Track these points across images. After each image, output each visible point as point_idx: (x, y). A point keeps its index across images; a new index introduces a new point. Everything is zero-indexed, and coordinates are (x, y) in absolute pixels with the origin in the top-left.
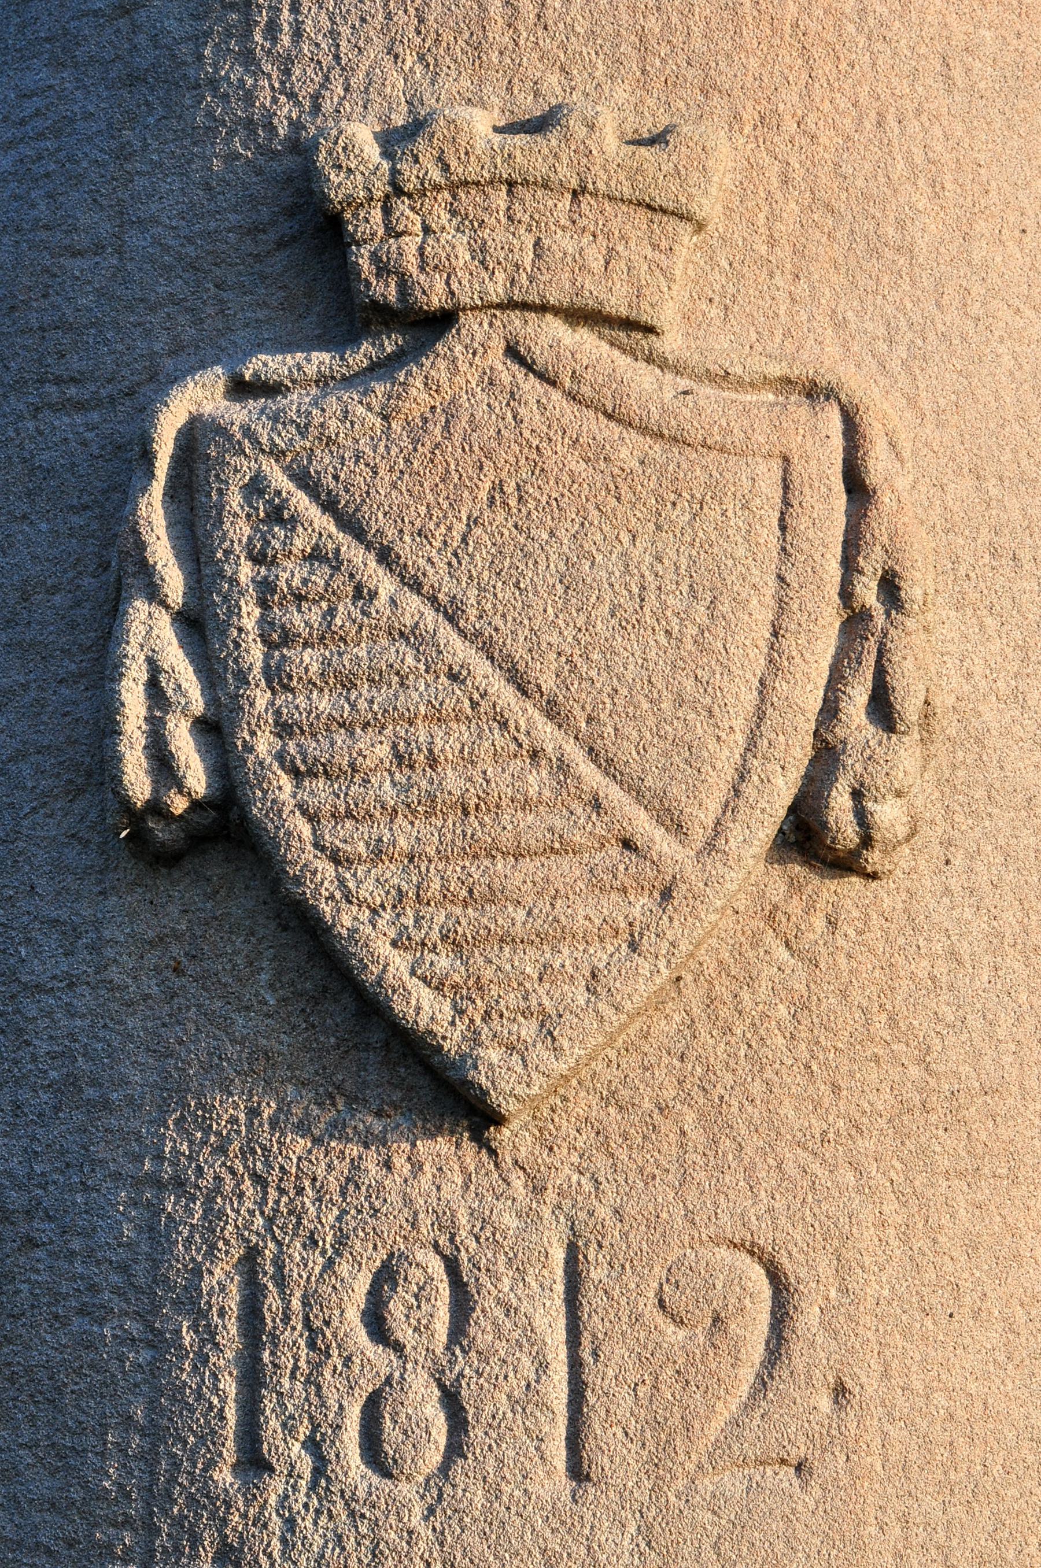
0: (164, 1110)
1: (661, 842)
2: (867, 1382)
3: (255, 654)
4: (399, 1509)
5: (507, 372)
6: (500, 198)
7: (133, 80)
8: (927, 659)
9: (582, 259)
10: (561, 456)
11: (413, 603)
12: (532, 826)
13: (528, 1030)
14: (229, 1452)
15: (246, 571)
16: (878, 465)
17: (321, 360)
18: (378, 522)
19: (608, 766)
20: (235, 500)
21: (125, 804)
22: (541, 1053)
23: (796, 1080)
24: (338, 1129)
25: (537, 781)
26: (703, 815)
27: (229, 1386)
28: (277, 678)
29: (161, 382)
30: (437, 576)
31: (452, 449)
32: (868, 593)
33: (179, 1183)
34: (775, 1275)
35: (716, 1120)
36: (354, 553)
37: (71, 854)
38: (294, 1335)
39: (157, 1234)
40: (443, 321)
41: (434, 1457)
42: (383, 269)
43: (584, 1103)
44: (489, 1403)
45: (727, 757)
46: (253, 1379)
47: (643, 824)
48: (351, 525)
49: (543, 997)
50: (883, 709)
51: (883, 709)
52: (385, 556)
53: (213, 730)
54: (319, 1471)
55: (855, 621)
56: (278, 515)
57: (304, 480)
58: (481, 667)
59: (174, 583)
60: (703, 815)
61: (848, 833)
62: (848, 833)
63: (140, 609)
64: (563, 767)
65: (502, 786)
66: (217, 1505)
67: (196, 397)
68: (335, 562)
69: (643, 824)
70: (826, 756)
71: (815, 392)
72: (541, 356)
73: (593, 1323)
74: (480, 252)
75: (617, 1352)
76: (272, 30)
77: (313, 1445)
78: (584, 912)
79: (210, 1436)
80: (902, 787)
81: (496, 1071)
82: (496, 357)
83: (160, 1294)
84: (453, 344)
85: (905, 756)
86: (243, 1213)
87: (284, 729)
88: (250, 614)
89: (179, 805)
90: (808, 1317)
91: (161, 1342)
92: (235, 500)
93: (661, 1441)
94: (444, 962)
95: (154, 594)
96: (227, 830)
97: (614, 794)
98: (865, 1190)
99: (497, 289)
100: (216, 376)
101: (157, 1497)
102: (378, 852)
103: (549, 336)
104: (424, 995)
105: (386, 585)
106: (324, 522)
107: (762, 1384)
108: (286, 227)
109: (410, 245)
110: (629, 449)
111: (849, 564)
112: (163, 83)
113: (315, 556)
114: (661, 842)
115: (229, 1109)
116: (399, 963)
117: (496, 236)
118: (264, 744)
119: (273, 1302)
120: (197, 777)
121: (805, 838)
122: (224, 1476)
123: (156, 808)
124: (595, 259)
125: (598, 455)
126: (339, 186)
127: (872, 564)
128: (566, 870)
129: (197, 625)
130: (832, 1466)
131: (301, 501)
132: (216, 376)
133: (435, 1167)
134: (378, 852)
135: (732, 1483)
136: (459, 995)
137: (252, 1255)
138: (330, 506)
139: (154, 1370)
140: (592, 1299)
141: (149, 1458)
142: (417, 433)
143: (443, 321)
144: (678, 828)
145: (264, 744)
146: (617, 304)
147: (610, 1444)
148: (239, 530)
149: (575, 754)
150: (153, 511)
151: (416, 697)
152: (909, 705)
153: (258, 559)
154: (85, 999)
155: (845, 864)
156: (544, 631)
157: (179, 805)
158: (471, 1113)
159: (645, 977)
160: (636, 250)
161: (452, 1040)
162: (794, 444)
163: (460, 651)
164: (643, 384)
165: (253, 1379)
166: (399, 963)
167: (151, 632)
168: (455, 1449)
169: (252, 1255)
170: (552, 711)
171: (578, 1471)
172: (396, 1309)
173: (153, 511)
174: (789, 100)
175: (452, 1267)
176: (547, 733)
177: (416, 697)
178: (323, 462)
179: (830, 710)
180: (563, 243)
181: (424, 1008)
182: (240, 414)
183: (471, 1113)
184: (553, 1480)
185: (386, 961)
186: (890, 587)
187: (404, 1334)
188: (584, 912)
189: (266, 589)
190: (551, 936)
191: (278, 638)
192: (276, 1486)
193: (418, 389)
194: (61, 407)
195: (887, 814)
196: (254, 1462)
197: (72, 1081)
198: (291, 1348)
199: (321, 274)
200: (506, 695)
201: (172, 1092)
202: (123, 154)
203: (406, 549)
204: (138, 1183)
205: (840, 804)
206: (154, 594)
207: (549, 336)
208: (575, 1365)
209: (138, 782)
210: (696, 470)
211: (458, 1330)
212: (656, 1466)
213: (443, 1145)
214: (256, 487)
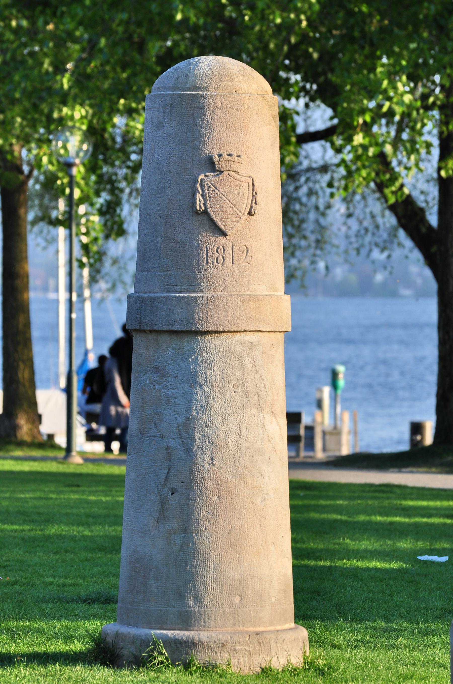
0: (199, 234)
1: (240, 214)
2: (253, 256)
3: (208, 198)
4: (219, 266)
5: (228, 176)
6: (228, 162)
7: (193, 148)
8: (259, 198)
9: (234, 167)
10: (232, 183)
11: (221, 195)
12: (230, 213)
13: (230, 229)
14: (205, 262)
15: (207, 191)
16: (255, 183)
17: (212, 174)
18: (218, 188)
19: (236, 208)
20: (206, 185)
21: (197, 210)
22: (231, 231)
23: (248, 232)
24: (214, 236)
25: (231, 209)
26: (243, 212)
27: (205, 256)
28: (210, 200)
29: (199, 175)
30: (223, 192)
31: (224, 182)
32: (254, 194)
33: (200, 240)
34: (245, 246)
35: (243, 236)
36: (216, 190)
37: (189, 213)
38: (211, 252)
39: (198, 245)
40: (223, 171)
41: (222, 262)
42: (218, 167)
43: (233, 234)
44: (226, 258)
45: (245, 207)
46: (207, 256)
47: (239, 213)
48: (215, 188)
49: (231, 226)
50: (256, 203)
51: (256, 203)
52: (219, 191)
53: (204, 204)
54: (213, 263)
55: (253, 196)
56: (209, 187)
57: (212, 184)
58: (226, 200)
59: (201, 192)
60: (243, 212)
61: (253, 213)
62: (253, 213)
63: (198, 194)
64: (233, 208)
65: (228, 209)
66: (204, 266)
67: (202, 176)
68: (215, 191)
69: (239, 213)
70: (251, 207)
71: (250, 177)
72: (231, 175)
73: (234, 252)
74: (226, 166)
75: (236, 254)
76: (207, 145)
77: (212, 261)
78: (234, 220)
79: (203, 261)
80: (257, 208)
81: (228, 232)
82: (227, 175)
83: (198, 249)
84: (224, 173)
85: (257, 207)
86: (206, 243)
87: (211, 204)
88: (207, 195)
89: (201, 210)
90: (249, 252)
91: (199, 253)
92: (206, 185)
93: (239, 261)
94: (224, 223)
95: (199, 193)
96: (206, 212)
97: (236, 210)
98: (253, 241)
99: (227, 169)
100: (203, 175)
101: (199, 265)
102: (218, 215)
103: (231, 173)
104: (222, 226)
105: (219, 193)
106: (213, 188)
107: (246, 257)
108: (208, 162)
109: (221, 165)
110: (237, 182)
111: (253, 191)
112: (196, 149)
113: (213, 190)
114: (240, 214)
115: (205, 234)
116: (220, 223)
117: (227, 165)
118: (209, 206)
119: (209, 250)
120: (203, 208)
121: (250, 213)
122: (205, 264)
123: (200, 210)
124: (235, 167)
125: (235, 183)
126: (215, 160)
127: (255, 191)
128: (233, 216)
129: (202, 195)
130: (251, 263)
131: (211, 186)
132: (203, 175)
133: (222, 239)
134: (218, 215)
135: (244, 264)
136: (225, 226)
137: (207, 246)
138: (214, 186)
139: (198, 255)
140: (234, 250)
141: (198, 262)
142: (221, 180)
143: (223, 171)
144: (241, 213)
145: (209, 206)
146: (237, 171)
147: (235, 261)
148: (206, 188)
149: (234, 207)
150: (198, 186)
151: (221, 202)
152: (257, 203)
153: (208, 190)
154: (191, 225)
155: (253, 215)
156: (231, 197)
157: (201, 210)
158: (225, 235)
159: (238, 225)
160: (238, 166)
161: (224, 230)
162: (249, 182)
163: (225, 199)
164: (238, 176)
165: (207, 256)
166: (220, 223)
167: (199, 196)
168: (223, 262)
169: (207, 246)
170: (232, 203)
171: (233, 263)
172: (219, 250)
173: (198, 186)
174: (247, 152)
175: (223, 247)
176: (231, 205)
177: (221, 202)
178: (213, 183)
179: (252, 203)
180: (233, 165)
181: (222, 227)
182: (206, 178)
183: (225, 235)
184: (231, 264)
185: (219, 223)
186: (256, 193)
187: (220, 253)
188: (234, 220)
189: (209, 193)
190: (232, 221)
191: (210, 197)
192: (209, 264)
193: (221, 177)
194: (187, 175)
195: (256, 211)
196: (207, 262)
197: (190, 232)
198: (210, 254)
199: (211, 165)
200: (228, 202)
201: (199, 233)
202: (192, 154)
203: (220, 190)
204: (196, 240)
205: (253, 211)
206: (199, 193)
207: (231, 173)
208: (232, 255)
209: (198, 208)
210: (242, 184)
211: (224, 252)
212: (238, 263)
213: (222, 238)
214: (207, 184)
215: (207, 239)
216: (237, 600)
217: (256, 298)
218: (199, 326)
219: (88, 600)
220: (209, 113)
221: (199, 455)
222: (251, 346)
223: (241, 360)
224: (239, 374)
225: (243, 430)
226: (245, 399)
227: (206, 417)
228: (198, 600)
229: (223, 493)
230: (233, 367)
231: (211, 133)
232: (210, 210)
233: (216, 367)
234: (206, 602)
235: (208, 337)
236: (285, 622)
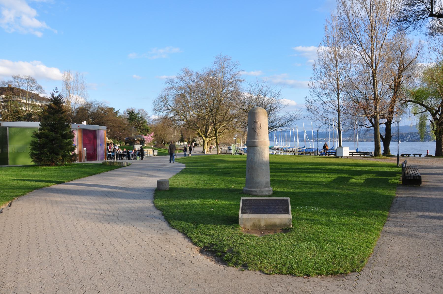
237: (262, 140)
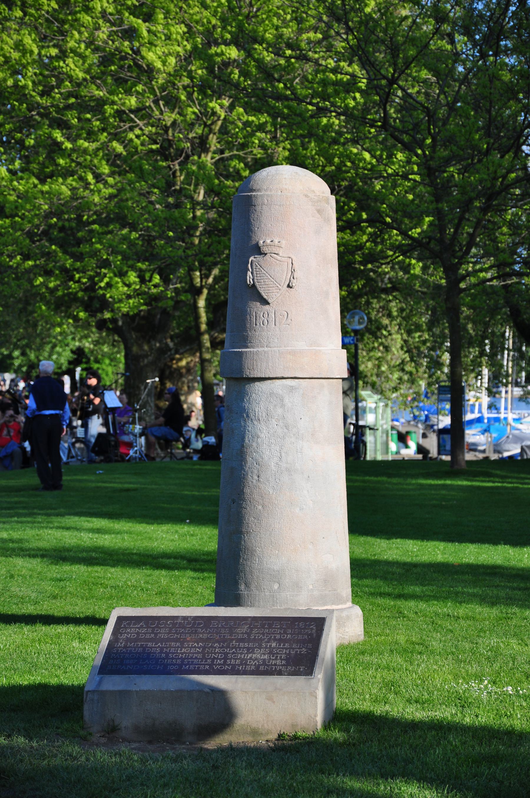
81: (270, 301)
85: (295, 281)
96: (254, 285)
121: (289, 286)
129: (252, 273)
133: (267, 307)
147: (277, 323)
164: (278, 258)
167: (249, 273)
181: (265, 297)
185: (263, 294)
199: (258, 250)
215: (256, 307)
216: (276, 586)
217: (293, 353)
218: (248, 373)
219: (456, 573)
220: (258, 208)
221: (250, 474)
222: (292, 389)
223: (282, 400)
224: (280, 411)
225: (283, 454)
226: (286, 430)
227: (254, 444)
228: (247, 585)
229: (266, 503)
230: (275, 406)
231: (260, 225)
232: (257, 284)
233: (262, 405)
234: (253, 587)
235: (257, 384)
236: (345, 603)
237: (301, 345)
